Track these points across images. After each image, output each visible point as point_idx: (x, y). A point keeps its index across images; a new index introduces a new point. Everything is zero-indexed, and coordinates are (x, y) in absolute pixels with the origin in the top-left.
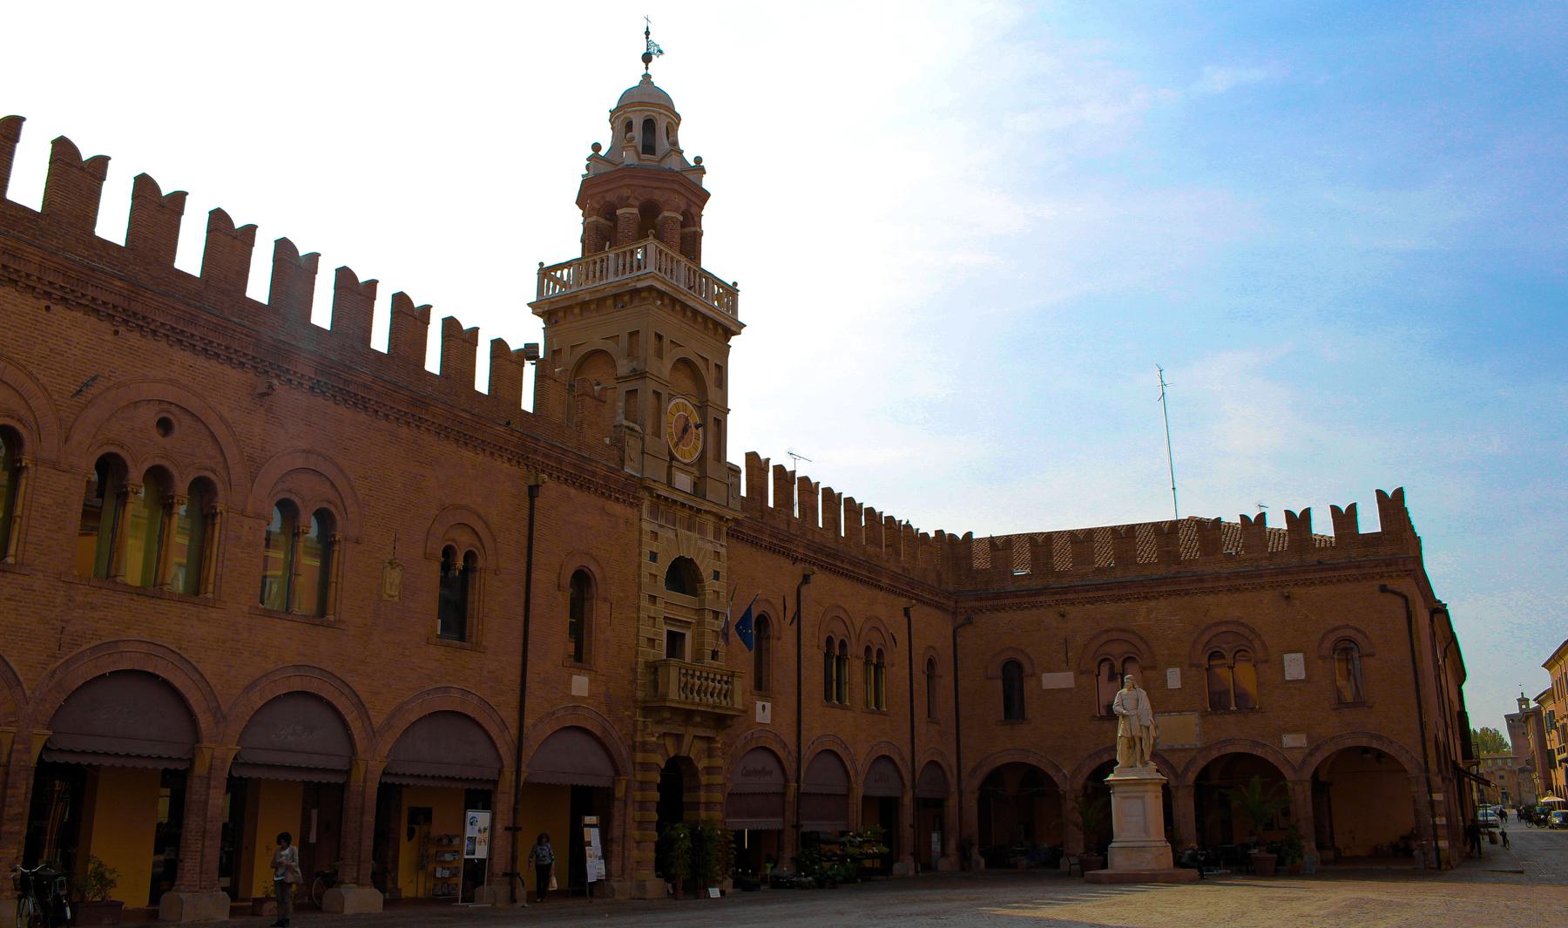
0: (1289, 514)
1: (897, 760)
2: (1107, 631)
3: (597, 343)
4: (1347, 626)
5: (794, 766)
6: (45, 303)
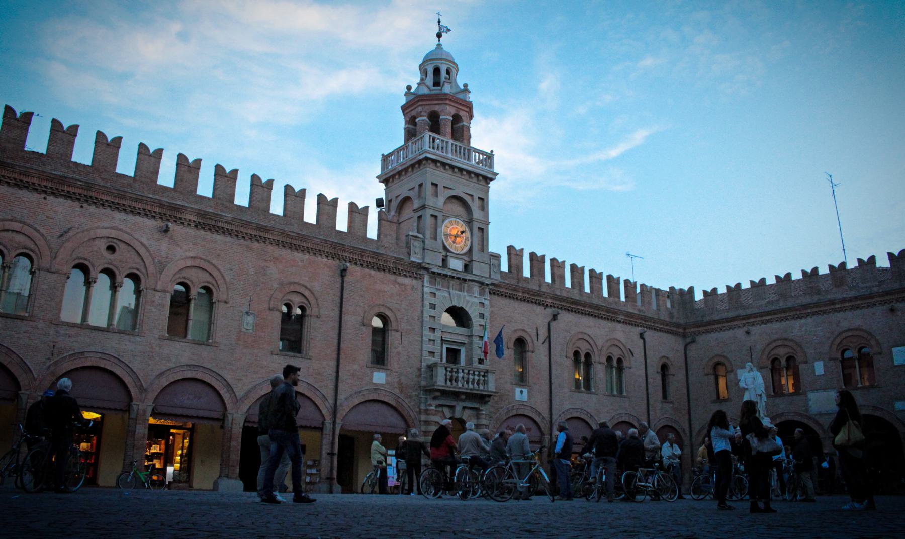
5: (548, 425)
6: (43, 195)
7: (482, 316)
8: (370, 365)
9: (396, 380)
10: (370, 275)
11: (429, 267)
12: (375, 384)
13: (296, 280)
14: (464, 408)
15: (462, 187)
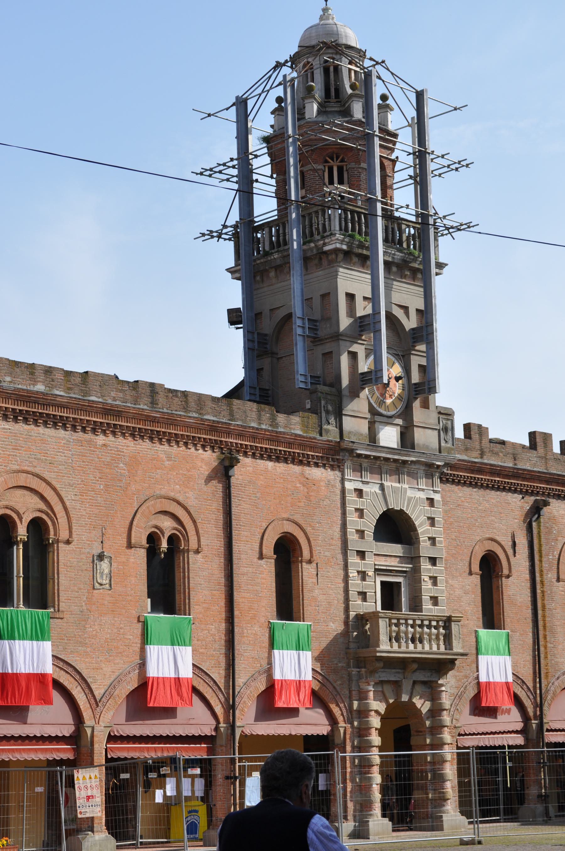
11: (354, 446)
14: (415, 683)
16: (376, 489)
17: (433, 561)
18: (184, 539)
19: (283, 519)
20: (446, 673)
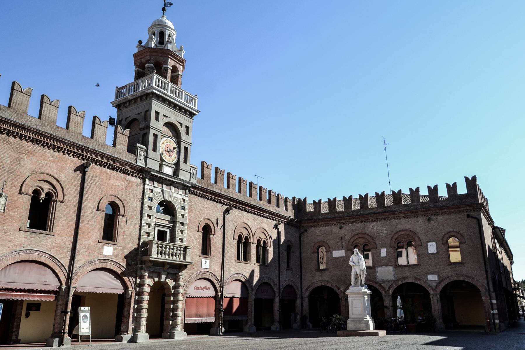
0: (429, 188)
1: (272, 284)
2: (357, 234)
3: (134, 116)
4: (453, 231)
7: (183, 208)
8: (101, 240)
9: (121, 252)
10: (106, 172)
12: (106, 256)
13: (46, 171)
15: (175, 117)
16: (160, 191)
17: (182, 224)
18: (55, 195)
19: (112, 195)
20: (183, 271)
